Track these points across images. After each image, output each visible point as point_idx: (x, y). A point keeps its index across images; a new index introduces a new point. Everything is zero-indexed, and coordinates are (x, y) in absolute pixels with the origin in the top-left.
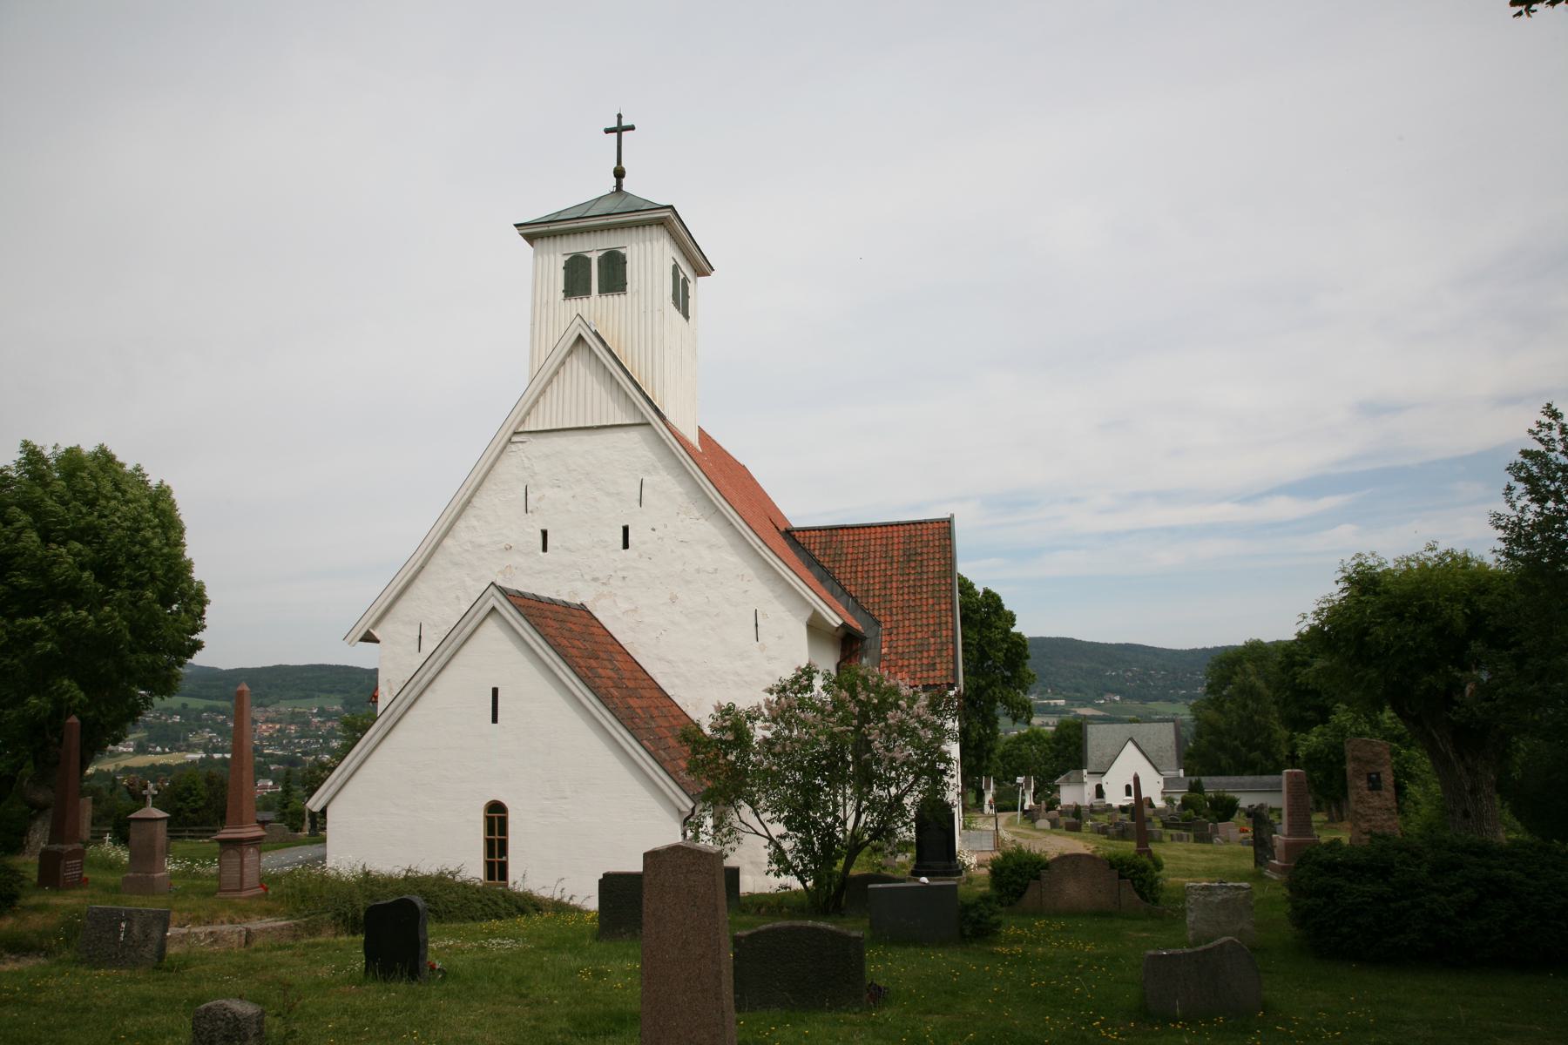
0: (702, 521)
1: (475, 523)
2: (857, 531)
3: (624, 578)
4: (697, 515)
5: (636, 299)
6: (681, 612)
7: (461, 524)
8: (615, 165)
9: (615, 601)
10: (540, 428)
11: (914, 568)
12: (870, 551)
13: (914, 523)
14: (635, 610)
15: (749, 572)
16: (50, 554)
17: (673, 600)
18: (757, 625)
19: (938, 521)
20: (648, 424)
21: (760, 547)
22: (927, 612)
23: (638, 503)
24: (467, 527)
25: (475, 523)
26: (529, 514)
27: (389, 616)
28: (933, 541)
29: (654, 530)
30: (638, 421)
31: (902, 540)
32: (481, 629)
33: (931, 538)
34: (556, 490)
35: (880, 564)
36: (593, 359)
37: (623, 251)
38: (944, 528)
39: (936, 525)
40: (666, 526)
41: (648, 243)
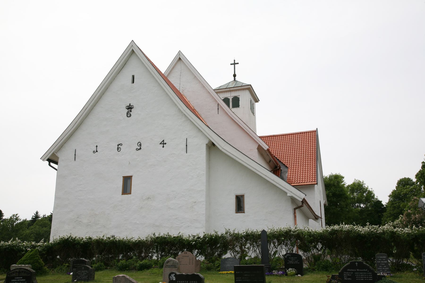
8: (234, 74)
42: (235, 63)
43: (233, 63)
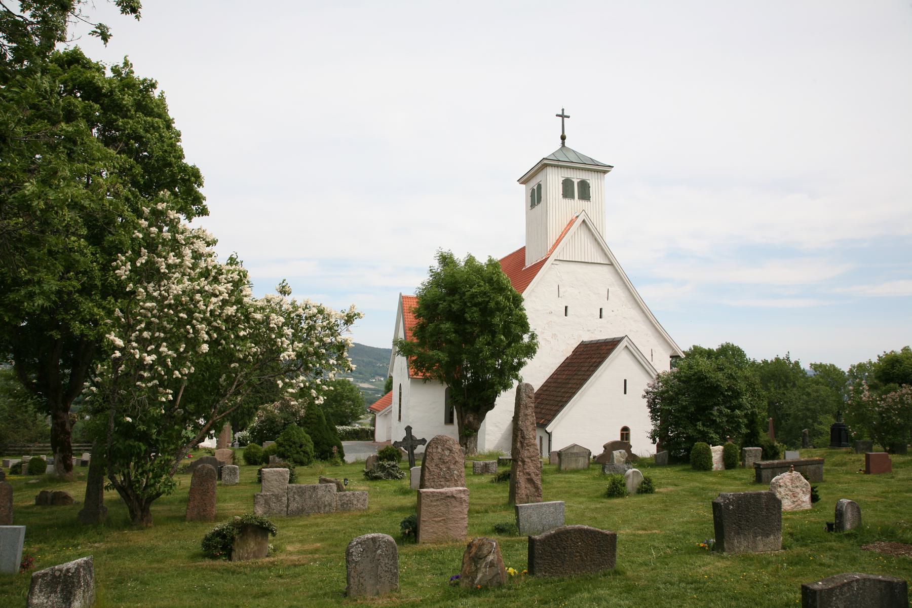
10: (565, 259)
20: (612, 264)
37: (588, 181)
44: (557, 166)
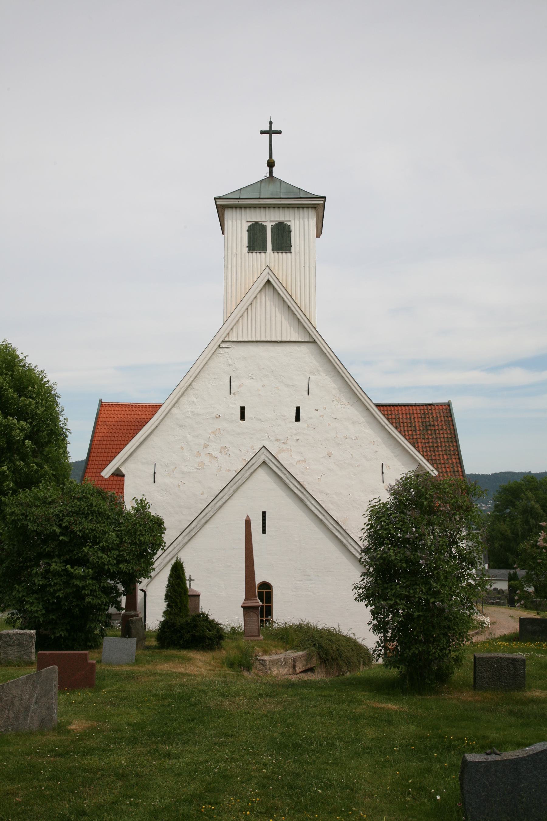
0: (348, 406)
1: (194, 399)
2: (389, 408)
3: (297, 440)
4: (345, 402)
5: (298, 257)
6: (335, 463)
7: (184, 400)
8: (268, 158)
9: (291, 455)
10: (240, 339)
11: (431, 434)
12: (400, 422)
13: (426, 405)
14: (304, 461)
15: (379, 440)
16: (9, 424)
17: (330, 455)
18: (383, 473)
19: (441, 405)
20: (314, 342)
21: (387, 425)
22: (444, 463)
23: (306, 393)
24: (189, 402)
25: (194, 399)
26: (232, 395)
27: (131, 458)
28: (440, 417)
29: (317, 410)
30: (307, 339)
31: (420, 416)
32: (254, 475)
33: (438, 415)
34: (251, 380)
35: (408, 431)
36: (276, 296)
37: (288, 223)
38: (446, 409)
39: (441, 407)
40: (325, 408)
41: (306, 220)
42: (273, 129)
43: (268, 129)
44: (240, 207)
